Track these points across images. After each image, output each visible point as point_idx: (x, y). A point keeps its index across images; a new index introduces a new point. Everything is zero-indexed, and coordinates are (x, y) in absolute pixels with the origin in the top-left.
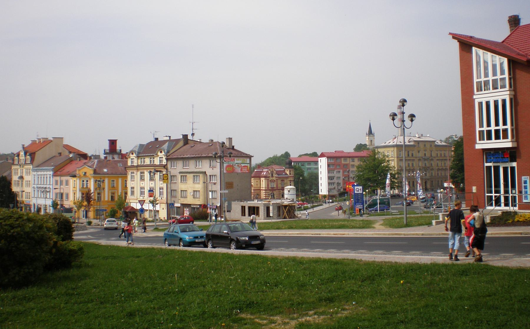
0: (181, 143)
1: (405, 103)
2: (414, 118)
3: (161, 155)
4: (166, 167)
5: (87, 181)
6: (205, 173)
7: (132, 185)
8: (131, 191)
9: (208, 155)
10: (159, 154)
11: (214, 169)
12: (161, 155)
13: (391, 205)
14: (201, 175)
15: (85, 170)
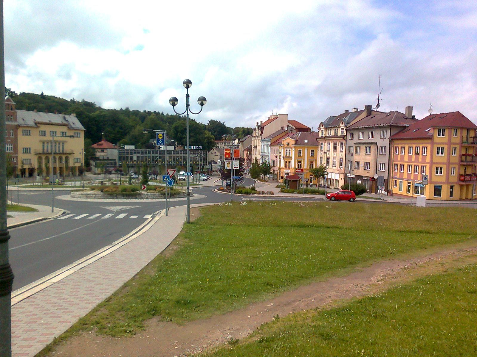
0: (364, 115)
1: (189, 85)
2: (176, 103)
3: (342, 127)
4: (345, 137)
5: (290, 151)
6: (376, 144)
7: (341, 156)
8: (320, 160)
9: (381, 125)
10: (341, 125)
11: (384, 140)
12: (342, 127)
13: (186, 201)
14: (372, 146)
15: (288, 141)
